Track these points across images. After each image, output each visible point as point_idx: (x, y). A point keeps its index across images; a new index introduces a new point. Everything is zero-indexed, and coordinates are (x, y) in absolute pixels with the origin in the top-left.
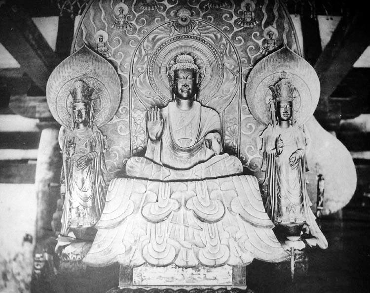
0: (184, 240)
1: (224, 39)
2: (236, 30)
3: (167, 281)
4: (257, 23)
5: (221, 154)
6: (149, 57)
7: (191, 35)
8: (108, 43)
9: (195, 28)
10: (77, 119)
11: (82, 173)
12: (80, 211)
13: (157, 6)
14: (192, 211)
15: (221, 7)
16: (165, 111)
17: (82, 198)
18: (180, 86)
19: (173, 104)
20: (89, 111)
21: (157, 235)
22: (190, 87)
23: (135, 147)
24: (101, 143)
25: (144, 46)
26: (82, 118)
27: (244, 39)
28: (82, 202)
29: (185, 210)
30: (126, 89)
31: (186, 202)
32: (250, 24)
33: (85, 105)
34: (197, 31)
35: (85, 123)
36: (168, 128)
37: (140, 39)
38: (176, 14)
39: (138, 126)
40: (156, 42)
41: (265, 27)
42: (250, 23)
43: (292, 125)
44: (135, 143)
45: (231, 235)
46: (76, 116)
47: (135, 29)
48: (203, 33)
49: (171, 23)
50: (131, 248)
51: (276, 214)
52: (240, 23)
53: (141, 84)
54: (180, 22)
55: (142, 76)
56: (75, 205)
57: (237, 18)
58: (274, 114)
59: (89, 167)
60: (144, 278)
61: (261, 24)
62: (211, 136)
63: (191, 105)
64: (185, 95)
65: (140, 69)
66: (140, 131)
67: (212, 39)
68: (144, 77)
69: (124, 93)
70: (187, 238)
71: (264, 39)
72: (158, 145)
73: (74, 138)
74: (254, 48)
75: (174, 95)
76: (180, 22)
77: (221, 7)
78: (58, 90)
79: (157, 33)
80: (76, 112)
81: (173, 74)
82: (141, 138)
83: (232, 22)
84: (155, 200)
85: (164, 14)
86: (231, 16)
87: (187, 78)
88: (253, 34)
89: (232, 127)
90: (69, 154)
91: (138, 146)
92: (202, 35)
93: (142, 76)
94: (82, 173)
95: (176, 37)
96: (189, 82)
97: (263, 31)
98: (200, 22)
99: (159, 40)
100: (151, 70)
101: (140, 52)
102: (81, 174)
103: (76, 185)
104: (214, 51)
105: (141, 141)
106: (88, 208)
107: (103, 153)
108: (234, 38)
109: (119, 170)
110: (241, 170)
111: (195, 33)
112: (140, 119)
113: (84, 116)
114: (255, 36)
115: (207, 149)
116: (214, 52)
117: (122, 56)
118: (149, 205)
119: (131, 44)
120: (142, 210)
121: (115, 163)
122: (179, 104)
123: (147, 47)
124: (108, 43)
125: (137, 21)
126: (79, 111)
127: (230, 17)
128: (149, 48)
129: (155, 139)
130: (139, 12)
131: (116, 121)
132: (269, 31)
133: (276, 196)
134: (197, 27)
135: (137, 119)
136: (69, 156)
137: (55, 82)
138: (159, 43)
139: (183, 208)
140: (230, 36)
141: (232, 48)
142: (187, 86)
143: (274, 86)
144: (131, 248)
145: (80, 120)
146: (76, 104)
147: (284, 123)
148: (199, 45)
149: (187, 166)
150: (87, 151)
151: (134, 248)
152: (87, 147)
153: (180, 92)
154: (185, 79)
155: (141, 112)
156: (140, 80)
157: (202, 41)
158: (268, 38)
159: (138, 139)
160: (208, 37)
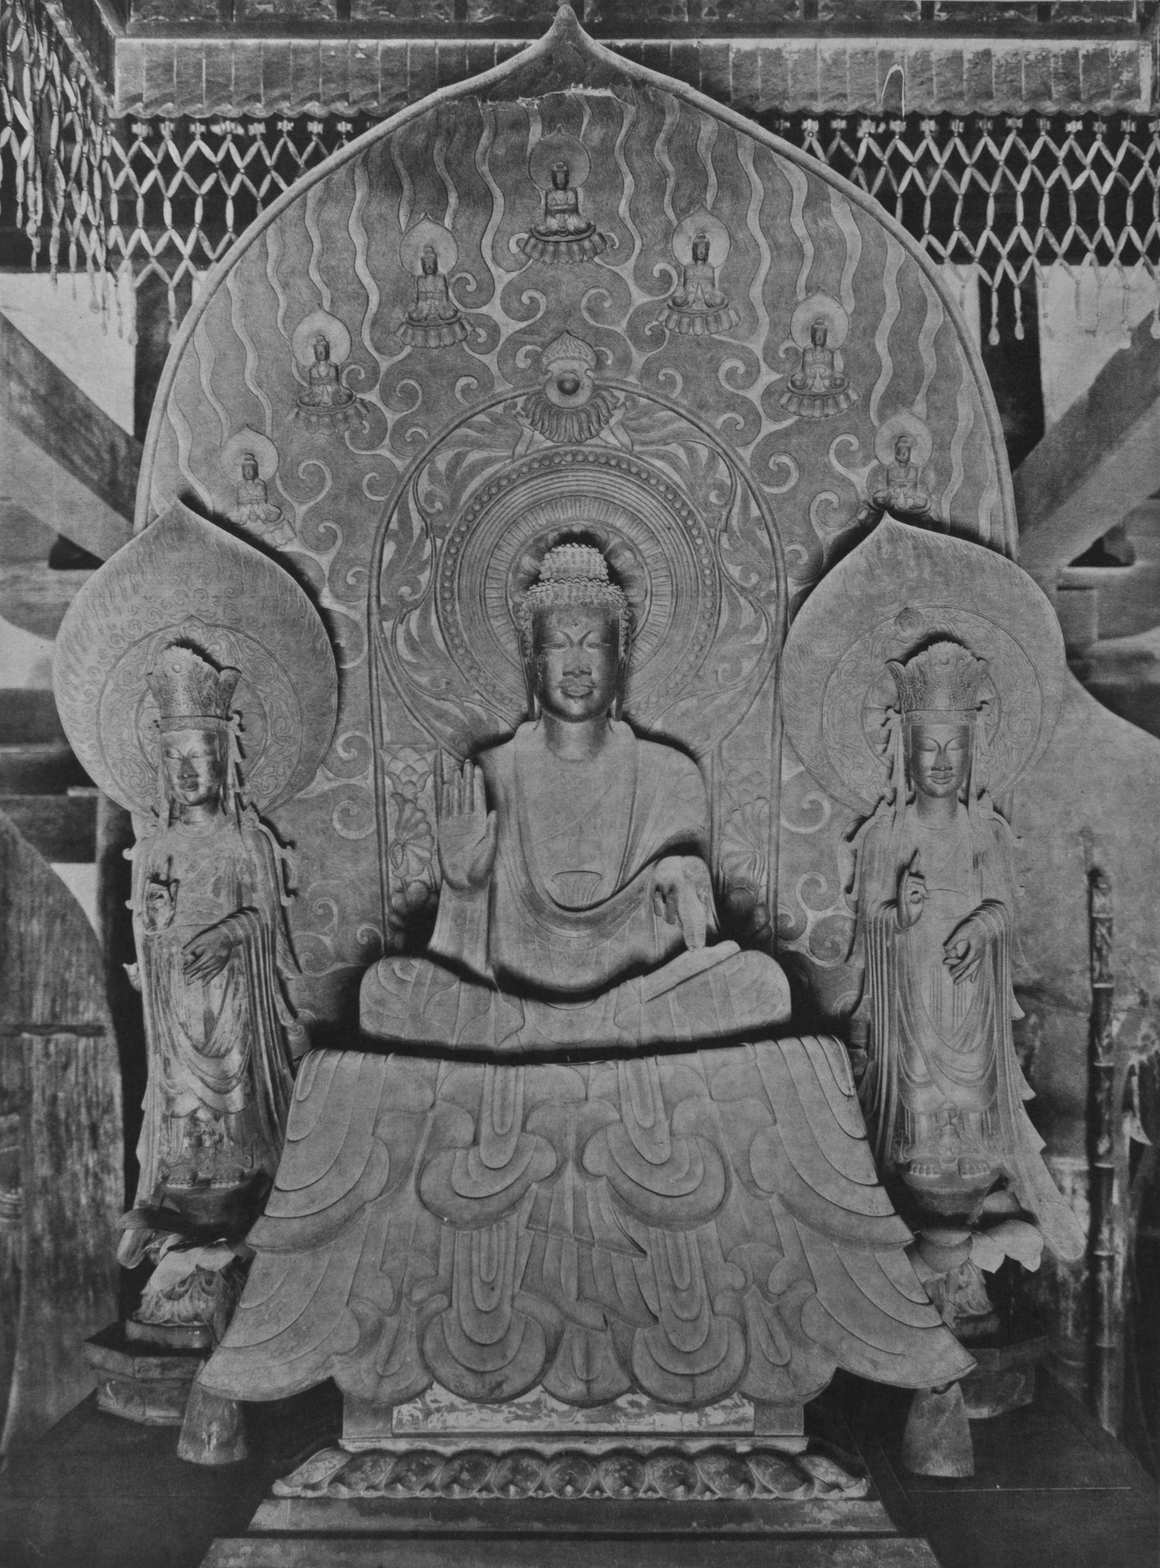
0: (578, 1299)
1: (722, 466)
2: (769, 427)
3: (518, 1417)
4: (854, 397)
5: (712, 939)
6: (439, 542)
7: (598, 450)
8: (278, 482)
9: (613, 421)
10: (178, 790)
11: (206, 993)
12: (203, 1127)
13: (463, 328)
14: (603, 1182)
15: (713, 328)
16: (501, 759)
17: (209, 1079)
18: (557, 675)
19: (530, 735)
20: (224, 757)
21: (475, 1279)
22: (596, 676)
23: (399, 884)
24: (276, 877)
25: (416, 500)
26: (195, 786)
27: (800, 467)
28: (209, 1096)
29: (576, 1175)
30: (358, 667)
31: (581, 1150)
32: (824, 405)
33: (209, 739)
34: (620, 433)
35: (213, 802)
36: (514, 828)
37: (399, 464)
38: (536, 358)
39: (408, 808)
40: (463, 485)
41: (882, 417)
42: (823, 398)
43: (965, 802)
44: (396, 867)
45: (750, 1278)
46: (176, 781)
47: (380, 423)
48: (644, 443)
49: (520, 402)
50: (380, 1326)
51: (890, 1131)
52: (784, 401)
53: (413, 646)
54: (554, 395)
55: (415, 615)
56: (185, 1105)
57: (775, 377)
58: (900, 765)
59: (232, 970)
60: (433, 1406)
61: (867, 399)
62: (674, 868)
63: (597, 739)
64: (576, 707)
65: (405, 590)
66: (417, 824)
67: (673, 461)
68: (424, 618)
69: (350, 681)
70: (589, 1291)
71: (875, 463)
72: (479, 902)
73: (170, 860)
74: (835, 505)
75: (536, 702)
76: (554, 395)
77: (713, 328)
78: (101, 678)
79: (465, 441)
80: (175, 765)
81: (529, 624)
82: (418, 851)
83: (754, 394)
84: (469, 1137)
85: (490, 360)
86: (752, 374)
87: (581, 643)
88: (834, 446)
89: (748, 808)
90: (152, 923)
91: (408, 879)
92: (637, 448)
93: (414, 617)
94: (206, 993)
95: (540, 461)
96: (594, 659)
97: (874, 431)
98: (630, 396)
99: (473, 471)
100: (447, 595)
101: (405, 522)
102: (201, 997)
103: (182, 1034)
104: (684, 513)
105: (420, 859)
106: (233, 1117)
107: (283, 909)
108: (761, 459)
109: (340, 966)
110: (781, 1008)
111: (612, 440)
112: (415, 778)
113: (204, 779)
114: (844, 454)
115: (660, 921)
116: (678, 512)
117: (335, 537)
118: (444, 1159)
119: (370, 486)
120: (419, 1178)
121: (327, 941)
122: (552, 738)
123: (430, 498)
124: (278, 482)
125: (385, 397)
126: (186, 761)
127: (748, 373)
128: (438, 505)
129: (466, 882)
130: (392, 355)
131: (327, 787)
132: (897, 432)
133: (895, 1080)
134: (618, 415)
135: (404, 779)
136: (155, 929)
137: (85, 650)
138: (474, 484)
139: (570, 1171)
140: (746, 453)
141: (753, 504)
142: (583, 672)
143: (904, 663)
144: (380, 1326)
145: (192, 796)
146: (173, 733)
147: (939, 807)
148: (631, 494)
149: (587, 977)
150: (220, 906)
151: (392, 1322)
152: (224, 893)
153: (557, 696)
154: (576, 649)
155: (417, 757)
156: (408, 632)
157: (644, 479)
158: (888, 458)
159: (409, 853)
160: (662, 457)
